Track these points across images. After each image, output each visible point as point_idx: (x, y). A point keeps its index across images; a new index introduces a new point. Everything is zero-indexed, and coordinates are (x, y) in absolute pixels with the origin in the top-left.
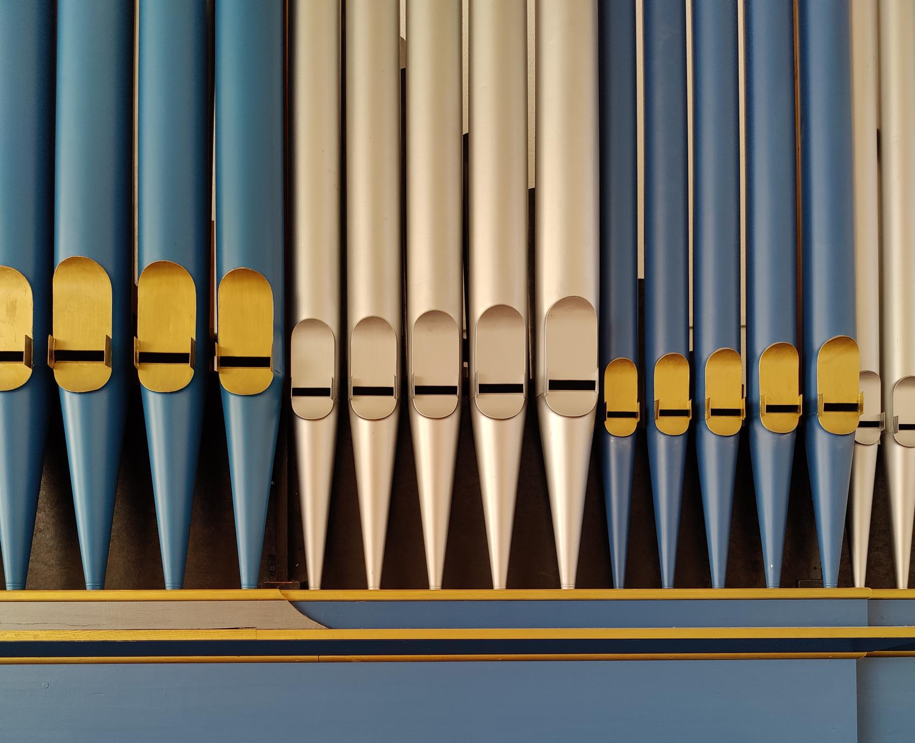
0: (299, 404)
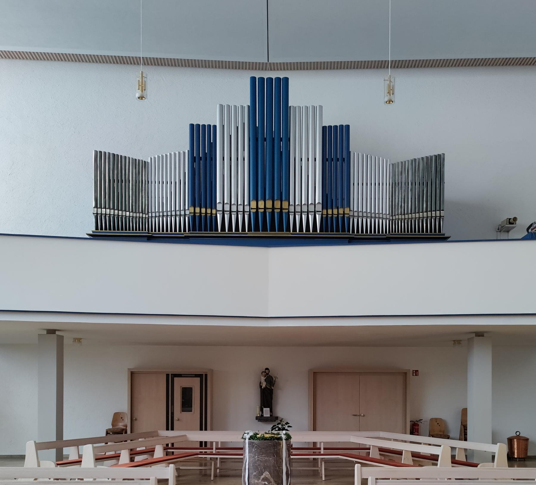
0: (290, 213)
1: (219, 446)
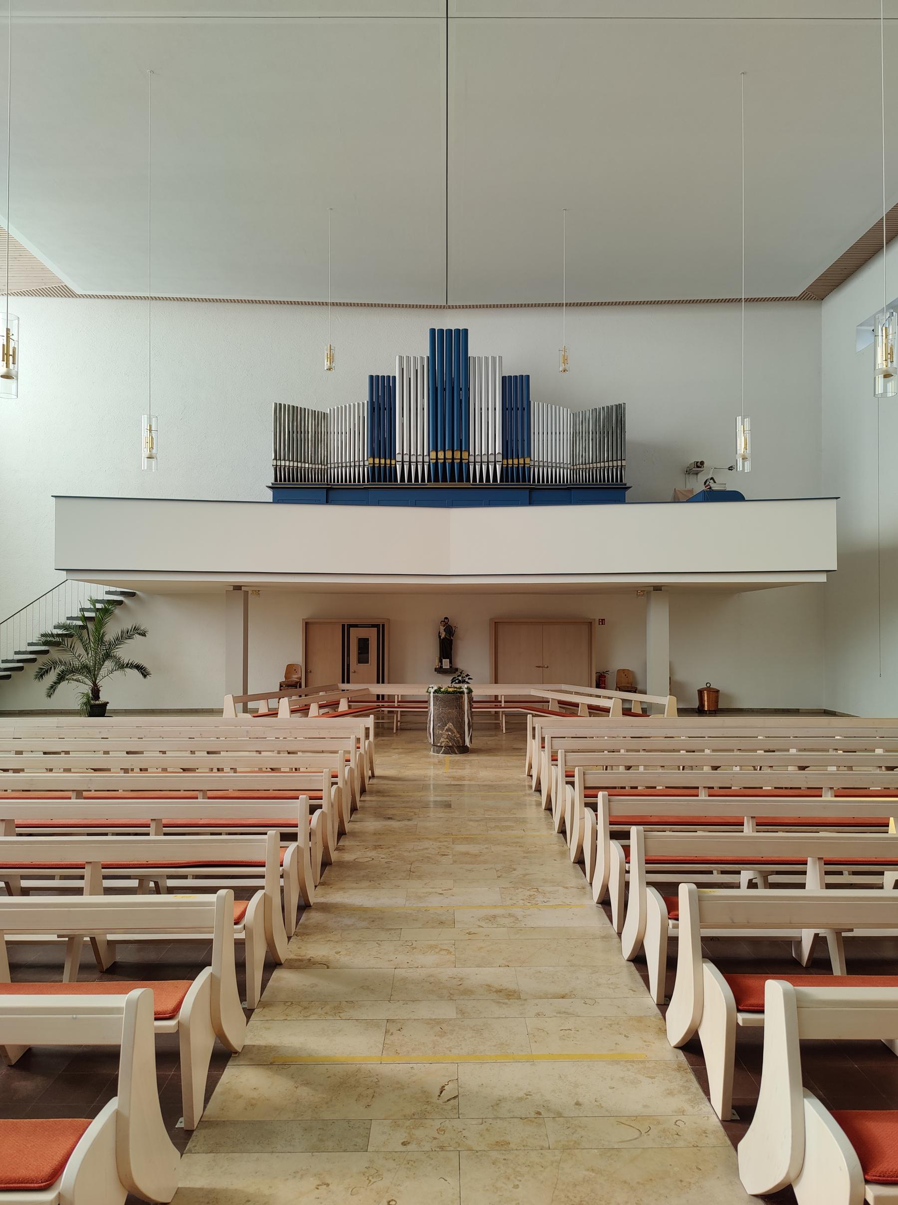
0: (470, 463)
1: (400, 700)
